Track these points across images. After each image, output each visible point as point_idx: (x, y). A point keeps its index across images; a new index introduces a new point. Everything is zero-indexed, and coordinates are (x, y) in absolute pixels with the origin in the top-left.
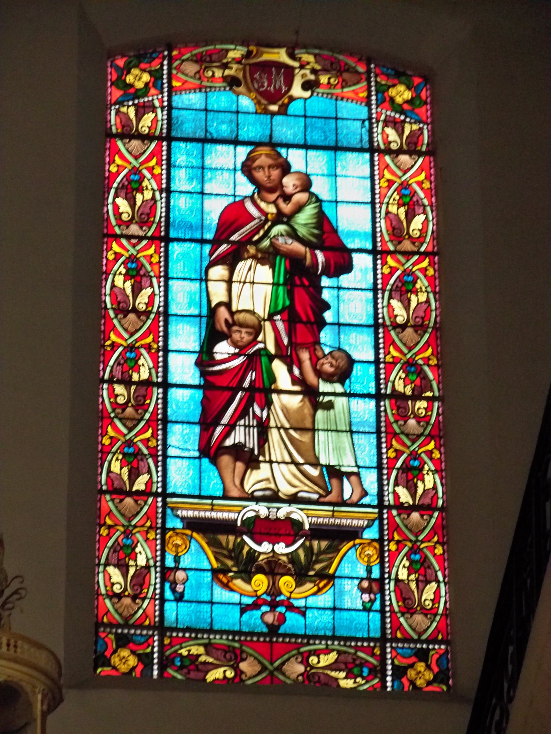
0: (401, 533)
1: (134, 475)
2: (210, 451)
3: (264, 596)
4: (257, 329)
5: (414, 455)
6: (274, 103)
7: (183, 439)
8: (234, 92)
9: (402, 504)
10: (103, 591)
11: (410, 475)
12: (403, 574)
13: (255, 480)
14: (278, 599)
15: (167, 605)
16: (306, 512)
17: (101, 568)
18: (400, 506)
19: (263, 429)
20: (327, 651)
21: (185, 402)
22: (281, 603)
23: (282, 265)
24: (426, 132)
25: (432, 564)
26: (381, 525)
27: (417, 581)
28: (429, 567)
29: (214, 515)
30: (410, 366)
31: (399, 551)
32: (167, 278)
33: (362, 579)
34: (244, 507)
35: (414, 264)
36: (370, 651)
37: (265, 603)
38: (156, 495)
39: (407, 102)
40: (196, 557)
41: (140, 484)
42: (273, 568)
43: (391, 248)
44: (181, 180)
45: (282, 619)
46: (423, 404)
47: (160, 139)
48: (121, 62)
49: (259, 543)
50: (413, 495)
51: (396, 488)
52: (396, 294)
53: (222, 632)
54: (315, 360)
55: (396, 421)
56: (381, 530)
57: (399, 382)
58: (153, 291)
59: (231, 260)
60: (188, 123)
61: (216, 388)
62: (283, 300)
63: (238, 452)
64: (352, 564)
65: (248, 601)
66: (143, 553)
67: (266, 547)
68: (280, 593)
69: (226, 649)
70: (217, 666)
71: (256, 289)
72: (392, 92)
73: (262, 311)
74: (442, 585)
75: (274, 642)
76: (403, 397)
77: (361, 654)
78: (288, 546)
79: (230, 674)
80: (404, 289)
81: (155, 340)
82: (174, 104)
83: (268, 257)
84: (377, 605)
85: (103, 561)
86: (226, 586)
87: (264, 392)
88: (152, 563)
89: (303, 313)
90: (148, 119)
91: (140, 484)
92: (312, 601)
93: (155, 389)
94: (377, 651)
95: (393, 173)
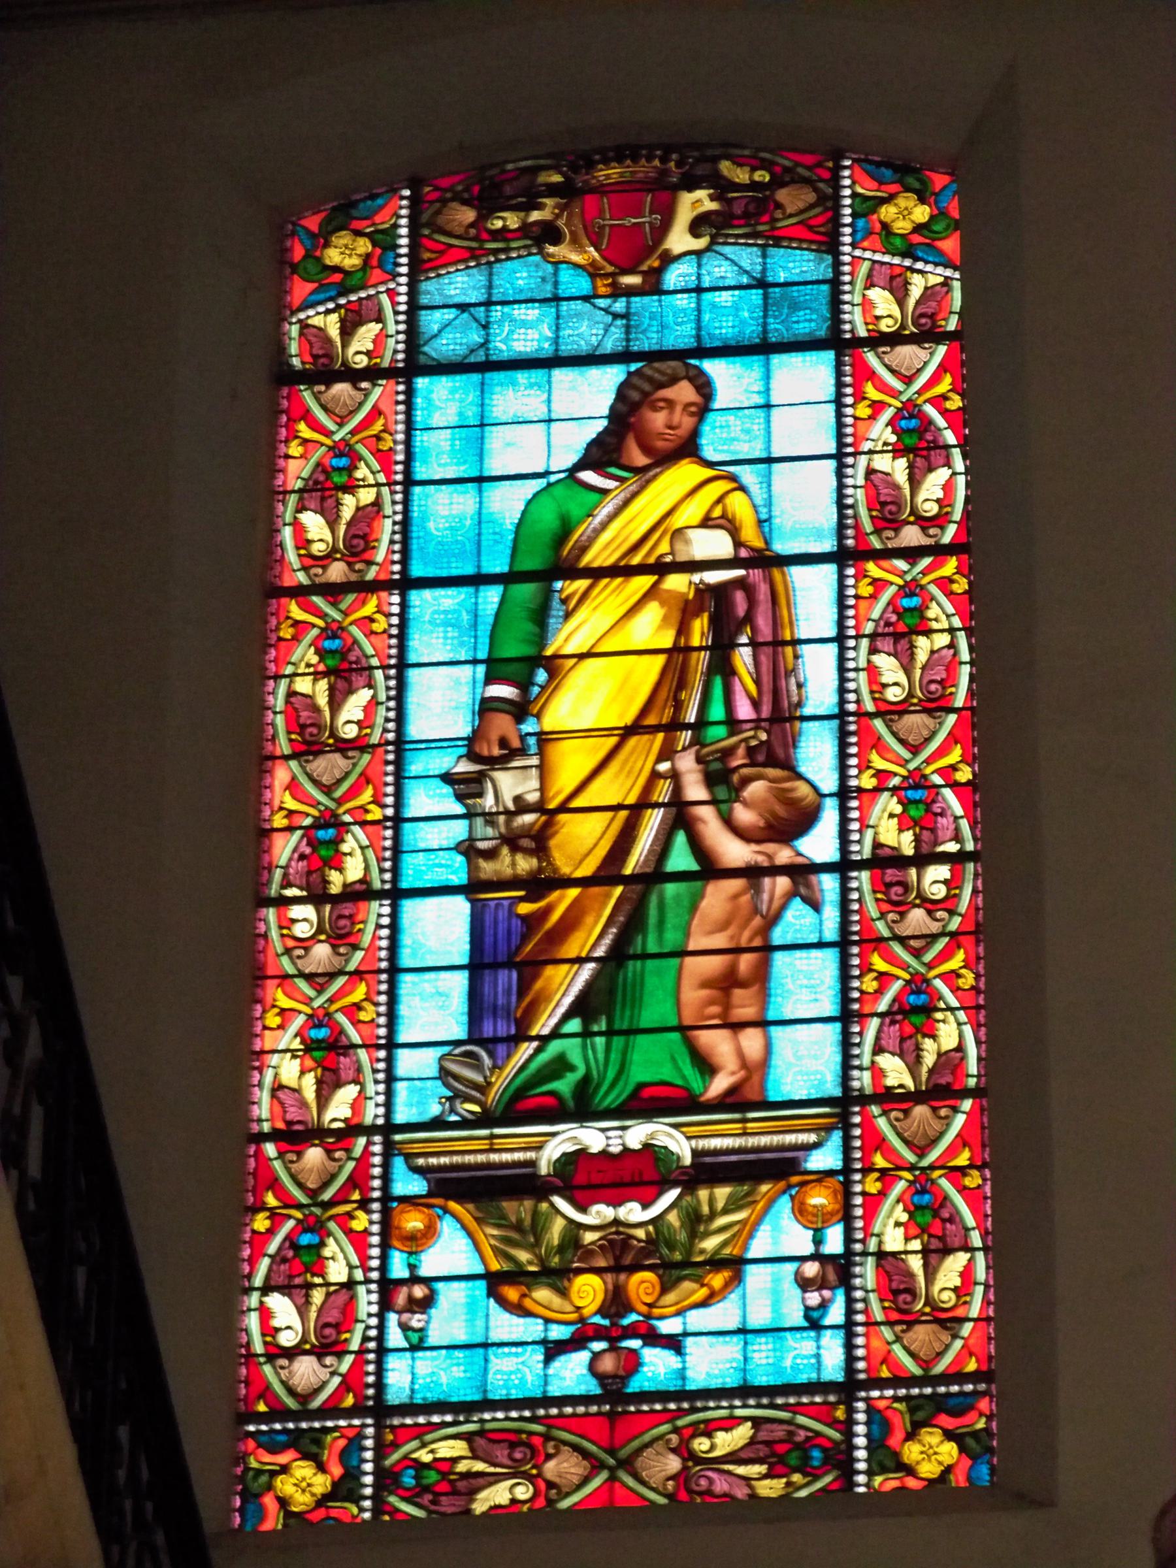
0: (889, 1152)
1: (326, 1088)
3: (597, 1320)
5: (918, 983)
6: (631, 271)
8: (546, 257)
9: (889, 1089)
10: (259, 1348)
12: (894, 1240)
14: (626, 1322)
15: (392, 1361)
16: (684, 1129)
17: (254, 1300)
18: (887, 1097)
20: (729, 1423)
22: (631, 1332)
24: (957, 285)
25: (958, 1212)
26: (847, 1139)
27: (925, 1252)
28: (951, 1220)
29: (495, 1157)
31: (883, 1194)
32: (403, 665)
33: (803, 1259)
34: (554, 1134)
35: (924, 573)
36: (823, 1414)
37: (599, 1333)
38: (371, 1130)
39: (919, 228)
41: (339, 1108)
43: (876, 543)
44: (437, 455)
45: (633, 1362)
46: (941, 871)
47: (391, 373)
48: (313, 222)
49: (583, 1208)
50: (914, 1066)
51: (878, 1059)
52: (886, 644)
53: (507, 1404)
55: (883, 915)
56: (847, 1149)
58: (374, 697)
60: (449, 337)
65: (559, 1333)
66: (340, 1256)
67: (600, 1213)
68: (629, 1308)
69: (511, 1439)
70: (497, 1478)
72: (887, 212)
74: (980, 1257)
76: (898, 861)
77: (801, 1420)
78: (646, 1206)
79: (523, 1492)
81: (377, 801)
84: (836, 1314)
85: (258, 1281)
86: (520, 1310)
88: (359, 1275)
90: (365, 336)
91: (339, 1108)
92: (697, 1319)
93: (375, 905)
94: (840, 1413)
95: (883, 387)
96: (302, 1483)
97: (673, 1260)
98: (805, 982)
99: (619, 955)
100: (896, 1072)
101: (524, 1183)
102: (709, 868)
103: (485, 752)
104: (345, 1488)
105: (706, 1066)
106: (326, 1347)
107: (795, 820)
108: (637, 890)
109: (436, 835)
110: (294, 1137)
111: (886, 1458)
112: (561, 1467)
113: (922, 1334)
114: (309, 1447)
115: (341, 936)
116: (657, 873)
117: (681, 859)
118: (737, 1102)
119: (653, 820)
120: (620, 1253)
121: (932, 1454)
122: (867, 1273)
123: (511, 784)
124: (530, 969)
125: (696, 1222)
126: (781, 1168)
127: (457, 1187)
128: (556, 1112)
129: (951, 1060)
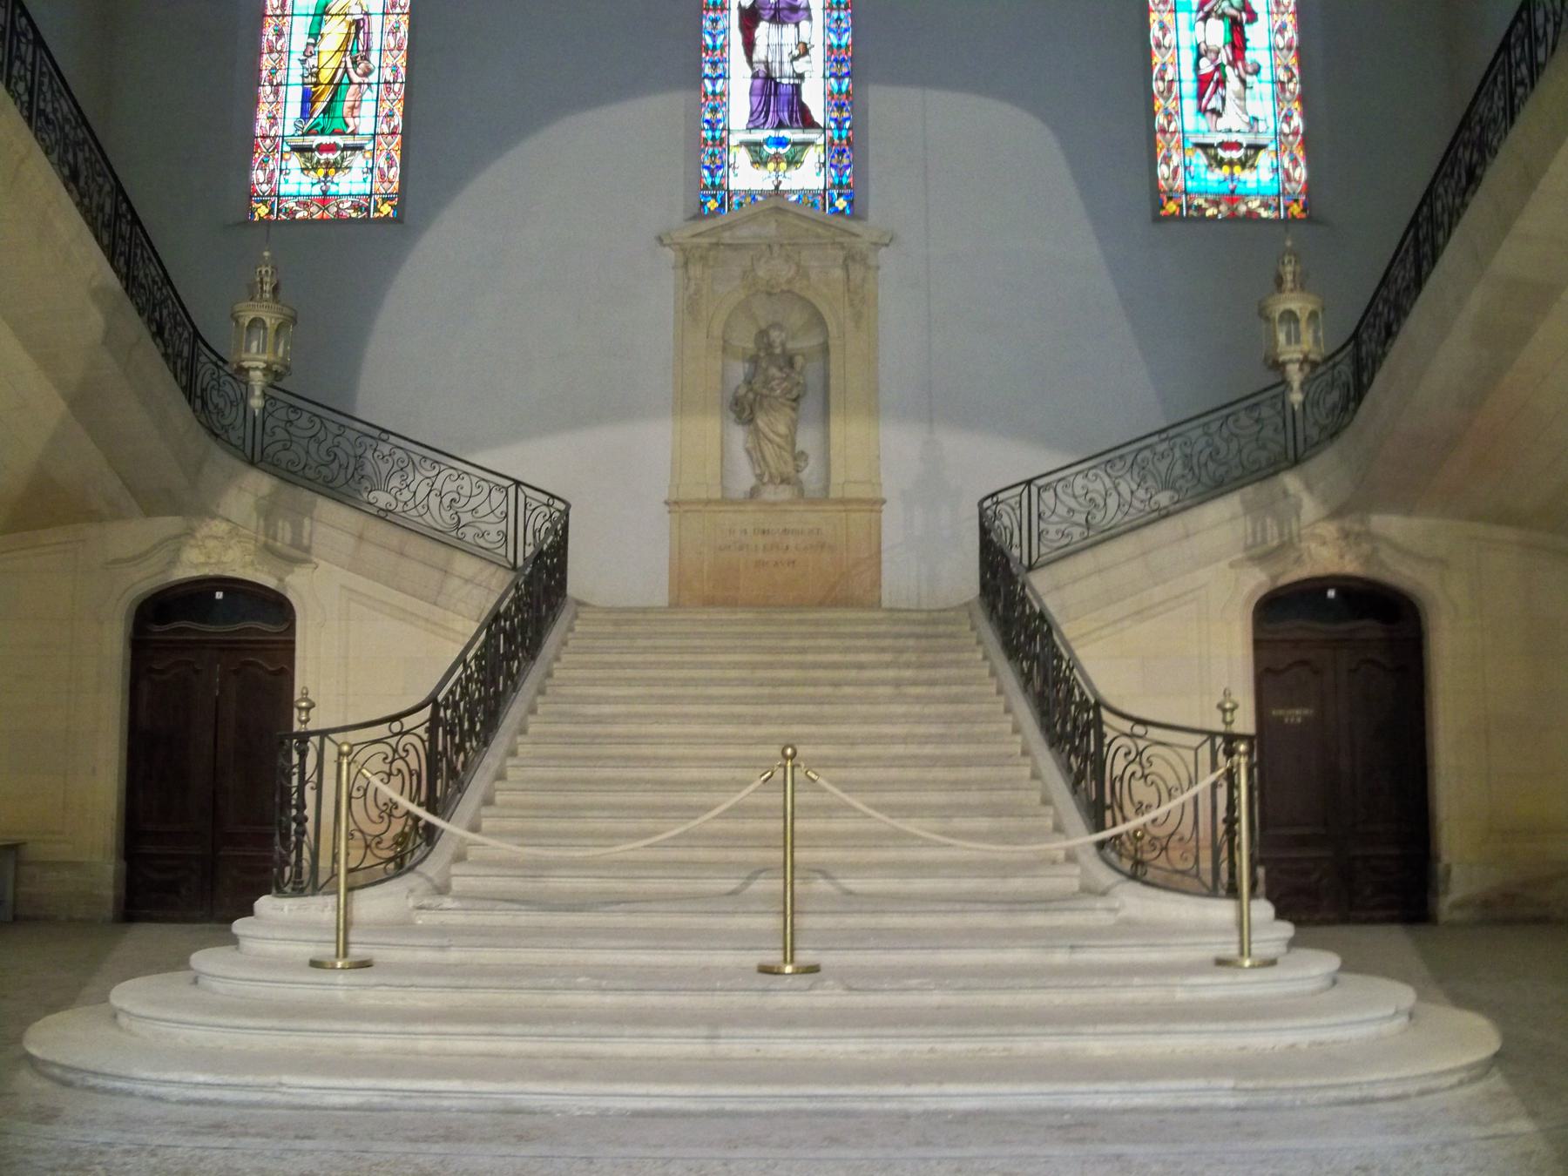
2: (1202, 110)
4: (1218, 53)
7: (1190, 105)
11: (1288, 118)
13: (1222, 123)
19: (1223, 99)
21: (1189, 87)
23: (1228, 21)
30: (1287, 68)
40: (1200, 159)
41: (1172, 128)
42: (1231, 163)
54: (1244, 66)
57: (1283, 76)
59: (1205, 19)
61: (1203, 82)
62: (1229, 38)
63: (1214, 111)
64: (1264, 160)
71: (1216, 33)
73: (1221, 45)
75: (1233, 198)
80: (1282, 30)
82: (781, 952)
83: (1222, 16)
87: (1222, 82)
89: (1238, 44)
96: (263, 210)
97: (337, 166)
98: (368, 109)
99: (331, 100)
100: (386, 130)
101: (309, 149)
102: (351, 83)
103: (307, 55)
104: (271, 212)
105: (347, 126)
106: (269, 182)
107: (367, 73)
108: (336, 87)
109: (296, 74)
110: (264, 137)
111: (377, 210)
112: (314, 209)
113: (386, 185)
114: (264, 203)
115: (276, 93)
116: (339, 84)
117: (346, 80)
118: (353, 133)
119: (340, 72)
120: (328, 165)
121: (386, 209)
122: (376, 171)
123: (312, 61)
124: (313, 103)
125: (343, 159)
126: (360, 148)
127: (295, 149)
128: (316, 134)
129: (396, 127)
